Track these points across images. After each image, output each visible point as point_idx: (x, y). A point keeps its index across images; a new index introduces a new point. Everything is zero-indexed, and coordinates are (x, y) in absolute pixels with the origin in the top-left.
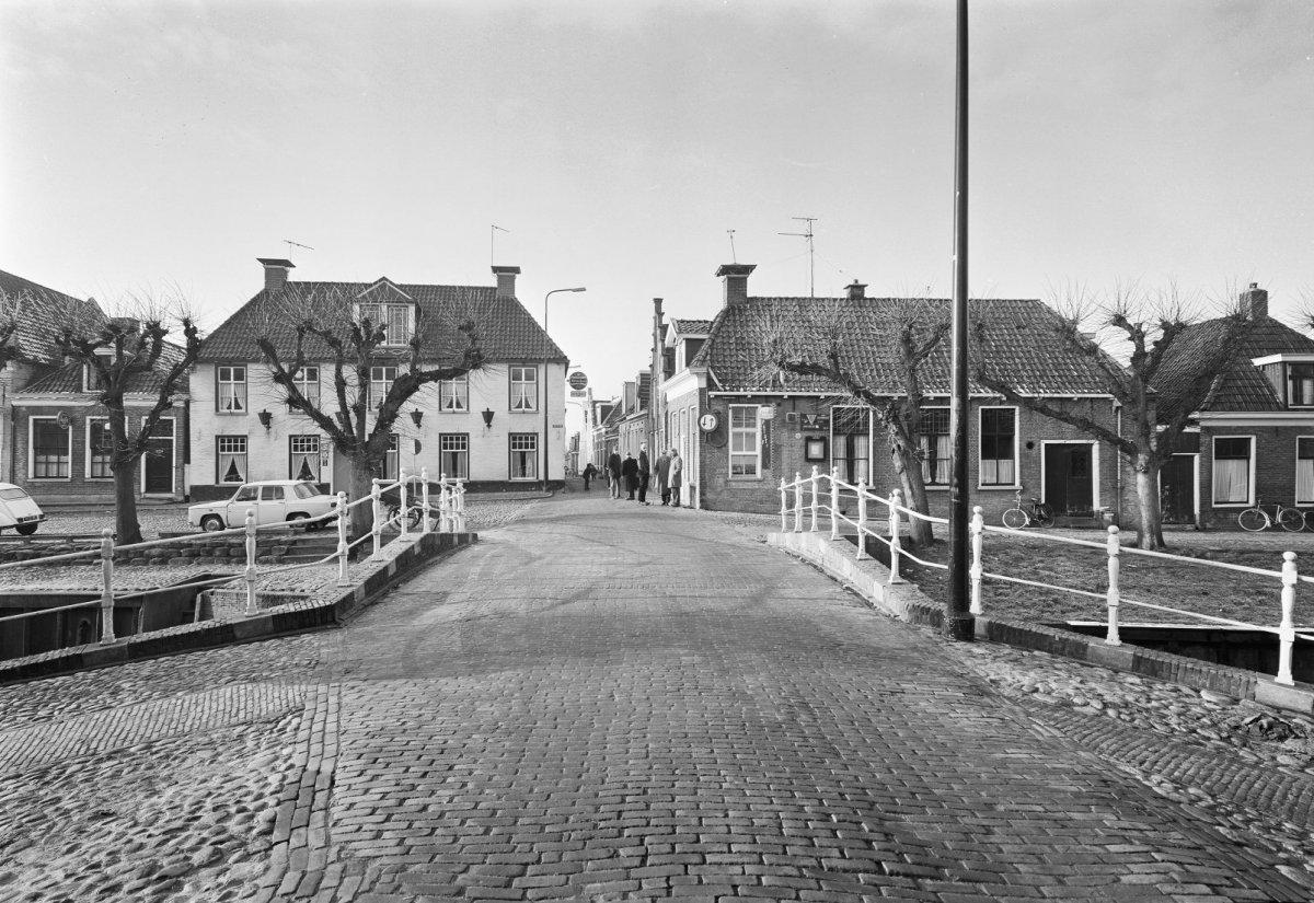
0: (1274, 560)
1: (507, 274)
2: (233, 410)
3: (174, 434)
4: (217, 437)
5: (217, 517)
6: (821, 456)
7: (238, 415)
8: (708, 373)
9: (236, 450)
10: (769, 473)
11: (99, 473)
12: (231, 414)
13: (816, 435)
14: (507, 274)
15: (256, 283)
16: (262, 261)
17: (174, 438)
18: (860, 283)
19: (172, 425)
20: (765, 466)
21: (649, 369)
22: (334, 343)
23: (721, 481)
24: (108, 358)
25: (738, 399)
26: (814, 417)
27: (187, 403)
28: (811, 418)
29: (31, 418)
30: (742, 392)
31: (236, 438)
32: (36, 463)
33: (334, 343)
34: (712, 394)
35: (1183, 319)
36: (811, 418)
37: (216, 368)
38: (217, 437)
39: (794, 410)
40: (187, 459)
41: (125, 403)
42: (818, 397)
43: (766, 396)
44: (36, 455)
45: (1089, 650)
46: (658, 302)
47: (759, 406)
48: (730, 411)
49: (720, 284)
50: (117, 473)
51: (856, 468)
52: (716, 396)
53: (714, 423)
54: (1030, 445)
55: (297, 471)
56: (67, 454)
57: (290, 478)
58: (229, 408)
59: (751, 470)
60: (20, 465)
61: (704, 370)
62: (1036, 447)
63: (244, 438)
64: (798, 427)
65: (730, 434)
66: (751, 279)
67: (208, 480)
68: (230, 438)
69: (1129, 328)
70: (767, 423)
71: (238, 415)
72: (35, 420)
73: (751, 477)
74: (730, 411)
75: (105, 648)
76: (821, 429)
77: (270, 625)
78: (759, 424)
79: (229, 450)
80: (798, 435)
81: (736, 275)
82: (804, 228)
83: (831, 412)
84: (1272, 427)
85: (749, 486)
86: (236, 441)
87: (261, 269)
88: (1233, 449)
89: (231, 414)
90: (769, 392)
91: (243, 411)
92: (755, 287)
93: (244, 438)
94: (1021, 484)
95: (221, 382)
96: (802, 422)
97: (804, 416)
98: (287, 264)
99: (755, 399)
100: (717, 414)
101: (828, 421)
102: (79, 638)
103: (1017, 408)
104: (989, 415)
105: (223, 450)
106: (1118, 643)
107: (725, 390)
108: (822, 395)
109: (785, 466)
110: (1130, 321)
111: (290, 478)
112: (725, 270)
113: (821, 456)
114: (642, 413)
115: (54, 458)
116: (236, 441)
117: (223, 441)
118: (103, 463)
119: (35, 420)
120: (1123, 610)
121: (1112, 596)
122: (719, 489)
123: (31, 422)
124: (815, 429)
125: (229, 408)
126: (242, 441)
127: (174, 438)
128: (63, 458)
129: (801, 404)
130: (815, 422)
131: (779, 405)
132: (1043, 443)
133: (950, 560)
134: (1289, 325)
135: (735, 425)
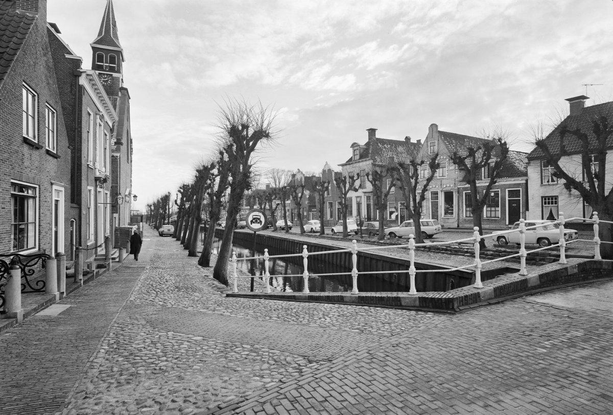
2: (550, 183)
3: (521, 197)
4: (542, 197)
5: (504, 237)
7: (553, 185)
9: (552, 203)
11: (489, 215)
12: (549, 185)
15: (564, 111)
16: (567, 100)
17: (521, 198)
19: (520, 192)
22: (583, 137)
24: (594, 156)
27: (527, 181)
29: (464, 192)
31: (552, 197)
32: (466, 211)
33: (583, 137)
37: (541, 162)
38: (542, 197)
40: (527, 209)
41: (477, 185)
44: (466, 207)
48: (98, 63)
50: (474, 215)
51: (574, 287)
55: (546, 215)
56: (499, 207)
57: (543, 219)
58: (548, 182)
60: (461, 212)
63: (556, 197)
65: (521, 197)
67: (342, 227)
68: (549, 197)
71: (553, 185)
72: (466, 193)
74: (98, 63)
75: (410, 296)
77: (417, 303)
79: (549, 204)
81: (372, 132)
86: (552, 199)
87: (568, 104)
89: (549, 185)
91: (556, 182)
92: (378, 135)
93: (556, 197)
98: (584, 97)
102: (450, 288)
105: (545, 203)
111: (543, 219)
115: (493, 209)
116: (552, 199)
117: (545, 199)
118: (491, 211)
119: (466, 193)
123: (464, 194)
125: (548, 182)
126: (556, 199)
127: (521, 198)
128: (497, 209)
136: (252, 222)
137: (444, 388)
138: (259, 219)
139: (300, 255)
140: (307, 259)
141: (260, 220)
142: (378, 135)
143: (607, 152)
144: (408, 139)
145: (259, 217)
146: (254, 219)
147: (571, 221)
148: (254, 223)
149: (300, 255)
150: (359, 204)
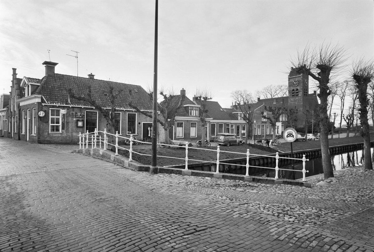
0: (216, 148)
1: (183, 89)
6: (78, 126)
8: (42, 97)
10: (64, 131)
13: (81, 119)
14: (183, 89)
18: (93, 74)
20: (63, 128)
21: (9, 94)
23: (46, 134)
25: (53, 106)
26: (80, 114)
28: (79, 114)
30: (54, 104)
31: (41, 143)
34: (43, 104)
35: (174, 95)
36: (79, 114)
39: (73, 111)
42: (81, 108)
43: (64, 106)
45: (182, 172)
46: (14, 70)
47: (61, 109)
48: (50, 111)
49: (43, 68)
52: (84, 108)
53: (39, 113)
54: (139, 123)
59: (58, 130)
61: (40, 96)
62: (141, 124)
64: (74, 117)
66: (56, 68)
69: (163, 95)
70: (64, 115)
73: (58, 132)
74: (50, 111)
76: (82, 117)
78: (61, 115)
80: (75, 119)
81: (50, 66)
82: (75, 54)
83: (85, 112)
84: (186, 120)
85: (57, 135)
88: (180, 125)
90: (64, 105)
92: (58, 70)
94: (137, 134)
95: (153, 111)
96: (76, 115)
97: (76, 113)
99: (59, 107)
100: (45, 111)
101: (84, 115)
103: (121, 113)
104: (129, 115)
106: (188, 169)
107: (48, 103)
108: (83, 107)
109: (70, 129)
110: (164, 94)
112: (45, 63)
113: (82, 126)
114: (4, 109)
120: (189, 161)
121: (187, 159)
122: (45, 137)
124: (80, 117)
129: (76, 110)
130: (80, 115)
131: (68, 109)
132: (143, 123)
133: (152, 153)
134: (145, 90)
135: (51, 115)
136: (287, 136)
137: (260, 194)
138: (292, 134)
139: (245, 154)
140: (305, 163)
141: (292, 135)
142: (58, 70)
143: (164, 99)
144: (11, 87)
145: (291, 133)
146: (288, 134)
147: (17, 106)
148: (289, 137)
149: (245, 154)
150: (82, 139)
